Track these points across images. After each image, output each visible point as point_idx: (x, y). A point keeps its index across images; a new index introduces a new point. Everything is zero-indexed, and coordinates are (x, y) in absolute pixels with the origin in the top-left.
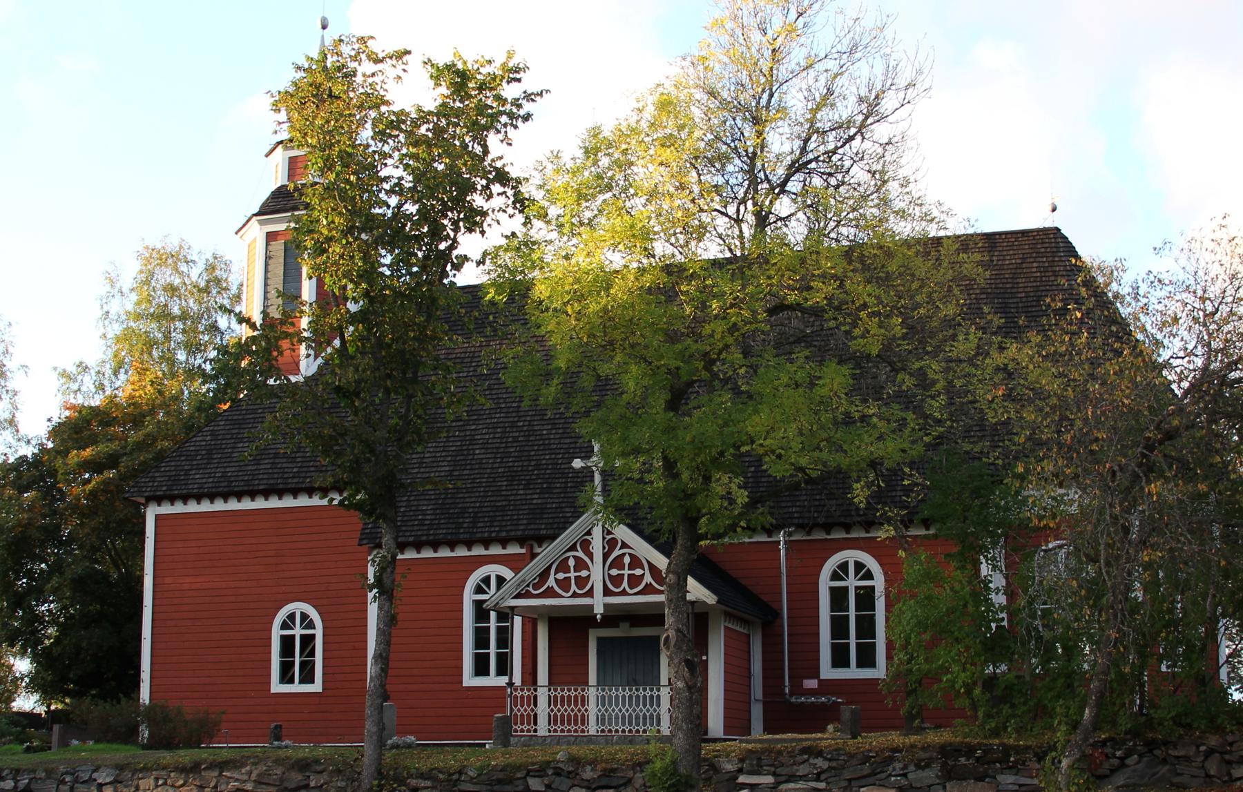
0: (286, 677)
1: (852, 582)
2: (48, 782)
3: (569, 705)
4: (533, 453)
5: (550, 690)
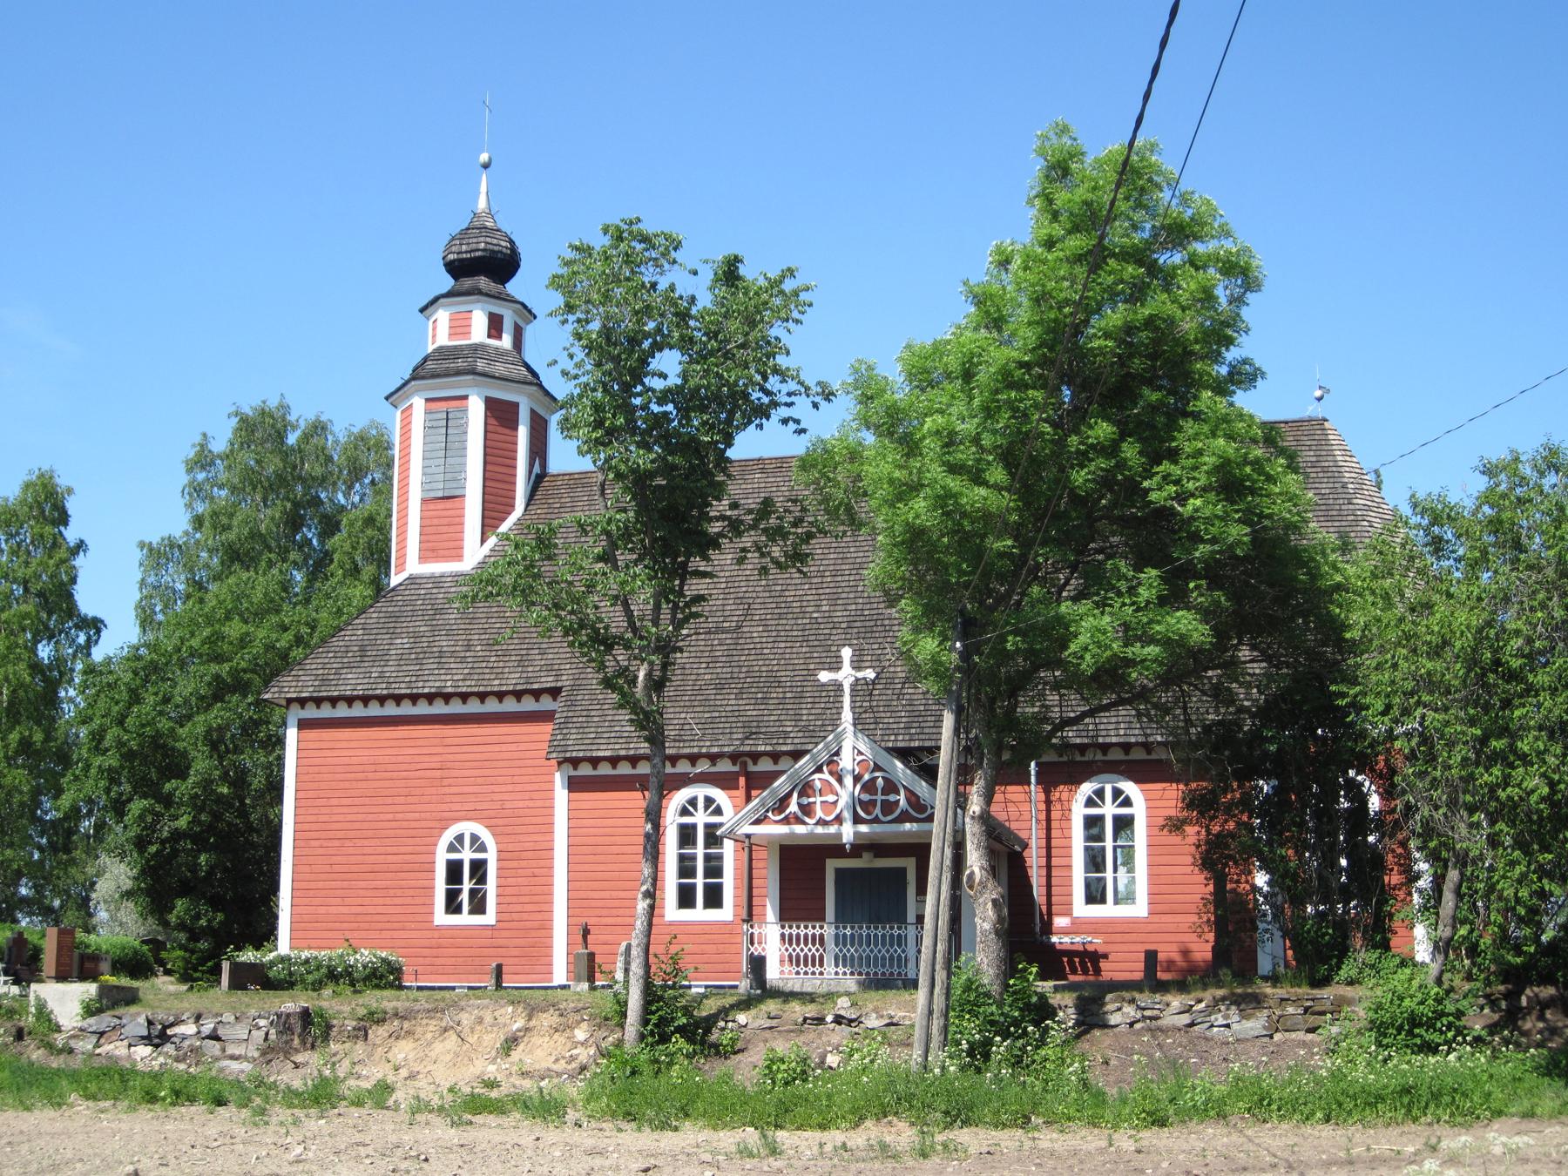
0: (453, 906)
1: (701, 818)
2: (238, 1027)
3: (798, 945)
4: (743, 658)
5: (837, 928)
